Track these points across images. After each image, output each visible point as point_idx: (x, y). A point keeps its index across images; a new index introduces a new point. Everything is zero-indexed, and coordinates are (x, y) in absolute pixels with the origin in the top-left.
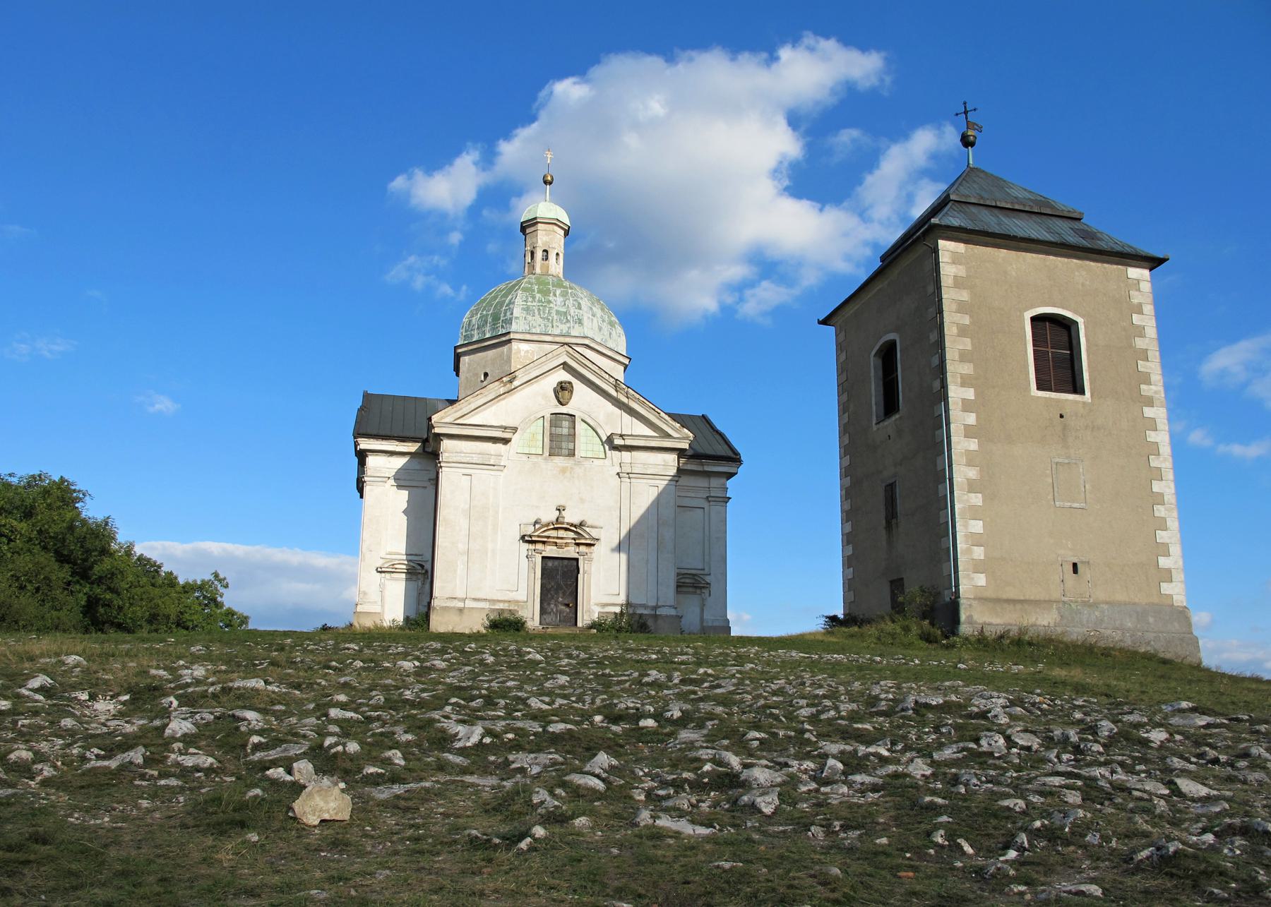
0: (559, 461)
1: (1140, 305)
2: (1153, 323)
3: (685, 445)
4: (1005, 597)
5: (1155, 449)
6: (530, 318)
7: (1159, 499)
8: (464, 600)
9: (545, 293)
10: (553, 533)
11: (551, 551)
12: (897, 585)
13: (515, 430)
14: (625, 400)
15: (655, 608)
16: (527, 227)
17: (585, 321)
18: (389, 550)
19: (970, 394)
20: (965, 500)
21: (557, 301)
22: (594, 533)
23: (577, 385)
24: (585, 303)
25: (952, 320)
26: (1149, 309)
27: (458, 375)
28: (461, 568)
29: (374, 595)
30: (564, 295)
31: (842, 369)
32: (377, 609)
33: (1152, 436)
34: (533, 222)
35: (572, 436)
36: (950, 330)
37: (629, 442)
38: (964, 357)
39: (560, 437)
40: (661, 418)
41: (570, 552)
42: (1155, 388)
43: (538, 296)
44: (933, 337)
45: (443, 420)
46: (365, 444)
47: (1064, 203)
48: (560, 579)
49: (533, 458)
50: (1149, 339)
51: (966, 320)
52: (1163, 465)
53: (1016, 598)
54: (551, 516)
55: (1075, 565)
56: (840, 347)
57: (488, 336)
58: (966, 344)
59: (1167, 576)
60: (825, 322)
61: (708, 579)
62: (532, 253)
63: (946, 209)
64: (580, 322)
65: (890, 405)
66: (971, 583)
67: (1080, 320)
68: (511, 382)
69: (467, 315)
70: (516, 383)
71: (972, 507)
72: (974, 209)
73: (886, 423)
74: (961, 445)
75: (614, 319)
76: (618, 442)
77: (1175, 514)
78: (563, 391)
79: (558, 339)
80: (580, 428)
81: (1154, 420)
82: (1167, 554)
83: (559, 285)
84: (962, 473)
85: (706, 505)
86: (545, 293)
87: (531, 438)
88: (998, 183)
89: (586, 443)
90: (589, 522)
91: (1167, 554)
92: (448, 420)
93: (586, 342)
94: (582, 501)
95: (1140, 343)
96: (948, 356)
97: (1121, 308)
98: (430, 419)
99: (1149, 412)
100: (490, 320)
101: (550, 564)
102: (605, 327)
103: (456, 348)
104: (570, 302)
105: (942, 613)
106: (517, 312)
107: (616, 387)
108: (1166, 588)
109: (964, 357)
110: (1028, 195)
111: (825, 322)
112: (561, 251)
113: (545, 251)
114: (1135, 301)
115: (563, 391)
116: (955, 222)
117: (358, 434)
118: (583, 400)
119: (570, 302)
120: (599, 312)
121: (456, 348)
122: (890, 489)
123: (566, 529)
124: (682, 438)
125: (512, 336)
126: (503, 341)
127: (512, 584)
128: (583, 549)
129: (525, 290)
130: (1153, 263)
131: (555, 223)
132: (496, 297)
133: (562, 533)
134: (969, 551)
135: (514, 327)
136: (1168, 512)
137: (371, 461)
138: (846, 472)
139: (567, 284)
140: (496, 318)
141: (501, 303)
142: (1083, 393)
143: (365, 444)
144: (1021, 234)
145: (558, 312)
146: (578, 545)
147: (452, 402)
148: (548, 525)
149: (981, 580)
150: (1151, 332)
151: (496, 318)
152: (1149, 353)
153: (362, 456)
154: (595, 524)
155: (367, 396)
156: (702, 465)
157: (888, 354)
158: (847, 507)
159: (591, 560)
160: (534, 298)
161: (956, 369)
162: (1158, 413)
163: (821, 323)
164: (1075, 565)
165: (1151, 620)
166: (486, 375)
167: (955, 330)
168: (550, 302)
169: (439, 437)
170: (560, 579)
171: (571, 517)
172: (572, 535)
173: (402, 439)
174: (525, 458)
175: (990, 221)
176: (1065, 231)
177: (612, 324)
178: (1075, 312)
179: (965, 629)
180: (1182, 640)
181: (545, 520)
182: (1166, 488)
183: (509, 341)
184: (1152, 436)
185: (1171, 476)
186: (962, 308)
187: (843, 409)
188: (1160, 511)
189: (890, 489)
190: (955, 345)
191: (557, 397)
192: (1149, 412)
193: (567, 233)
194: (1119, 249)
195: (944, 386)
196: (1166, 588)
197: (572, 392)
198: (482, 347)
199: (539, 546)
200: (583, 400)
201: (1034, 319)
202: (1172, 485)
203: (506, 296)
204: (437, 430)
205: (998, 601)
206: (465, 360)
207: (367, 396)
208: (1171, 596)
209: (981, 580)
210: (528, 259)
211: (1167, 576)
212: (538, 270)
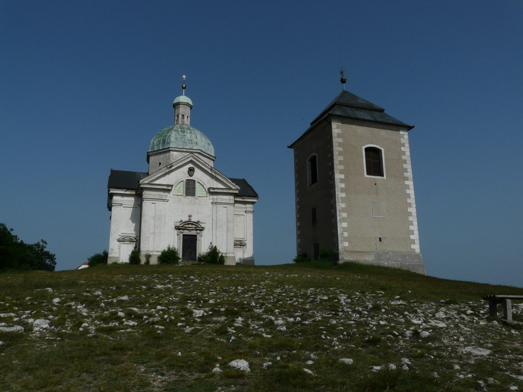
0: (190, 198)
1: (404, 143)
2: (410, 167)
3: (237, 192)
4: (355, 250)
5: (409, 196)
6: (177, 142)
7: (410, 214)
8: (152, 252)
9: (183, 132)
10: (187, 226)
11: (186, 232)
12: (316, 246)
13: (172, 186)
14: (214, 174)
15: (226, 253)
16: (176, 106)
17: (199, 143)
18: (123, 232)
19: (342, 176)
20: (341, 215)
21: (188, 136)
22: (203, 225)
23: (196, 169)
24: (199, 137)
25: (337, 149)
26: (407, 145)
27: (148, 162)
28: (151, 240)
29: (116, 250)
30: (191, 133)
31: (297, 165)
32: (118, 256)
33: (408, 191)
34: (178, 104)
35: (194, 188)
36: (336, 153)
37: (216, 191)
38: (341, 163)
39: (190, 188)
40: (228, 182)
41: (194, 233)
42: (409, 174)
43: (180, 133)
44: (329, 155)
45: (144, 182)
46: (112, 191)
47: (378, 103)
48: (190, 243)
49: (179, 197)
50: (407, 156)
51: (341, 149)
52: (412, 202)
53: (359, 250)
54: (186, 219)
55: (380, 239)
56: (296, 157)
57: (161, 148)
58: (341, 158)
59: (413, 242)
60: (290, 147)
61: (246, 242)
62: (178, 116)
63: (335, 107)
64: (197, 143)
65: (314, 180)
66: (343, 245)
67: (383, 149)
68: (171, 167)
69: (153, 140)
70: (173, 168)
71: (344, 218)
72: (345, 108)
73: (313, 186)
74: (340, 195)
75: (210, 142)
76: (211, 190)
77: (416, 220)
78: (191, 171)
79: (188, 150)
80: (197, 185)
81: (408, 185)
82: (413, 234)
83: (189, 129)
84: (340, 205)
85: (244, 214)
86: (183, 132)
87: (180, 189)
88: (355, 97)
89: (199, 190)
90: (201, 221)
91: (413, 234)
92: (146, 182)
93: (199, 151)
94: (198, 213)
95: (404, 157)
96: (335, 163)
97: (397, 147)
98: (139, 182)
99: (407, 183)
100: (161, 142)
101: (186, 237)
102: (206, 145)
103: (148, 153)
104: (193, 136)
105: (332, 255)
106: (172, 139)
107: (211, 169)
108: (413, 246)
109: (341, 163)
110: (364, 102)
111: (290, 147)
112: (189, 115)
113: (183, 115)
114: (402, 142)
115: (191, 171)
116: (338, 113)
117: (110, 186)
118: (198, 175)
119: (193, 136)
120: (204, 140)
121: (148, 153)
122: (314, 210)
123: (192, 224)
124: (235, 188)
125: (170, 149)
126: (168, 150)
127: (173, 241)
128: (198, 231)
129: (176, 131)
130: (408, 128)
131: (187, 104)
132: (164, 133)
133: (190, 226)
134: (342, 234)
135: (171, 145)
136: (413, 219)
137: (115, 198)
138: (298, 203)
139: (191, 128)
140: (164, 141)
141: (166, 136)
142: (383, 175)
143: (112, 191)
144: (361, 117)
145: (188, 140)
146: (197, 230)
147: (148, 174)
148: (185, 222)
149: (346, 244)
150: (408, 153)
151: (164, 141)
152: (407, 161)
153: (111, 196)
154: (204, 222)
155: (113, 172)
156: (243, 199)
157: (313, 160)
158: (298, 216)
159: (202, 236)
160: (179, 134)
161: (338, 167)
162: (410, 183)
163: (288, 147)
164: (380, 239)
165: (407, 258)
166: (160, 164)
167: (337, 153)
168: (185, 136)
169: (143, 189)
170: (190, 243)
171: (194, 219)
172: (194, 226)
173: (128, 189)
174: (176, 197)
175: (350, 112)
176: (377, 116)
177: (209, 144)
178: (381, 146)
179: (341, 262)
180: (418, 265)
181: (184, 220)
182: (413, 210)
183: (169, 151)
184: (405, 166)
185: (415, 206)
186: (340, 145)
187: (297, 179)
188: (411, 219)
189: (314, 210)
190: (337, 158)
191: (189, 173)
192: (407, 183)
193: (191, 108)
194: (397, 123)
195: (333, 174)
196: (413, 246)
197: (194, 171)
198: (158, 153)
199: (182, 231)
200: (198, 175)
201: (367, 150)
202: (415, 209)
203: (168, 132)
204: (142, 186)
205: (352, 252)
206: (152, 159)
207: (113, 172)
208: (414, 249)
209: (346, 244)
210: (176, 118)
211: (413, 242)
212: (180, 122)
